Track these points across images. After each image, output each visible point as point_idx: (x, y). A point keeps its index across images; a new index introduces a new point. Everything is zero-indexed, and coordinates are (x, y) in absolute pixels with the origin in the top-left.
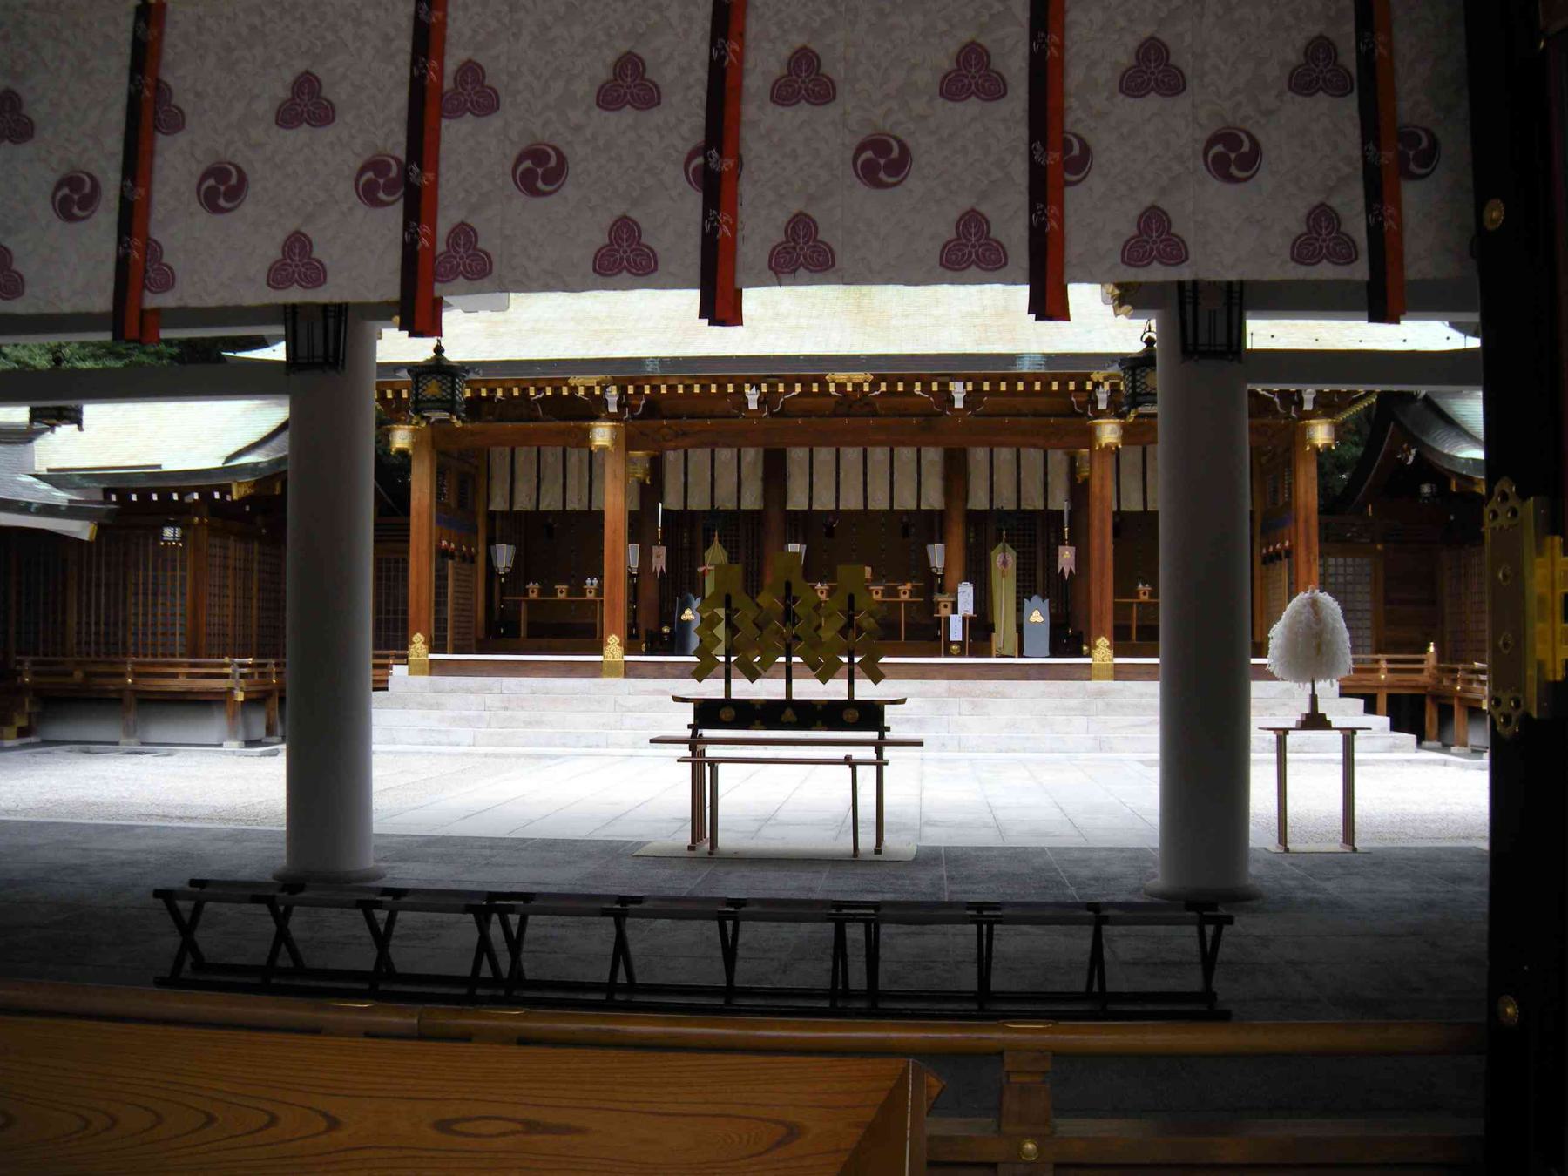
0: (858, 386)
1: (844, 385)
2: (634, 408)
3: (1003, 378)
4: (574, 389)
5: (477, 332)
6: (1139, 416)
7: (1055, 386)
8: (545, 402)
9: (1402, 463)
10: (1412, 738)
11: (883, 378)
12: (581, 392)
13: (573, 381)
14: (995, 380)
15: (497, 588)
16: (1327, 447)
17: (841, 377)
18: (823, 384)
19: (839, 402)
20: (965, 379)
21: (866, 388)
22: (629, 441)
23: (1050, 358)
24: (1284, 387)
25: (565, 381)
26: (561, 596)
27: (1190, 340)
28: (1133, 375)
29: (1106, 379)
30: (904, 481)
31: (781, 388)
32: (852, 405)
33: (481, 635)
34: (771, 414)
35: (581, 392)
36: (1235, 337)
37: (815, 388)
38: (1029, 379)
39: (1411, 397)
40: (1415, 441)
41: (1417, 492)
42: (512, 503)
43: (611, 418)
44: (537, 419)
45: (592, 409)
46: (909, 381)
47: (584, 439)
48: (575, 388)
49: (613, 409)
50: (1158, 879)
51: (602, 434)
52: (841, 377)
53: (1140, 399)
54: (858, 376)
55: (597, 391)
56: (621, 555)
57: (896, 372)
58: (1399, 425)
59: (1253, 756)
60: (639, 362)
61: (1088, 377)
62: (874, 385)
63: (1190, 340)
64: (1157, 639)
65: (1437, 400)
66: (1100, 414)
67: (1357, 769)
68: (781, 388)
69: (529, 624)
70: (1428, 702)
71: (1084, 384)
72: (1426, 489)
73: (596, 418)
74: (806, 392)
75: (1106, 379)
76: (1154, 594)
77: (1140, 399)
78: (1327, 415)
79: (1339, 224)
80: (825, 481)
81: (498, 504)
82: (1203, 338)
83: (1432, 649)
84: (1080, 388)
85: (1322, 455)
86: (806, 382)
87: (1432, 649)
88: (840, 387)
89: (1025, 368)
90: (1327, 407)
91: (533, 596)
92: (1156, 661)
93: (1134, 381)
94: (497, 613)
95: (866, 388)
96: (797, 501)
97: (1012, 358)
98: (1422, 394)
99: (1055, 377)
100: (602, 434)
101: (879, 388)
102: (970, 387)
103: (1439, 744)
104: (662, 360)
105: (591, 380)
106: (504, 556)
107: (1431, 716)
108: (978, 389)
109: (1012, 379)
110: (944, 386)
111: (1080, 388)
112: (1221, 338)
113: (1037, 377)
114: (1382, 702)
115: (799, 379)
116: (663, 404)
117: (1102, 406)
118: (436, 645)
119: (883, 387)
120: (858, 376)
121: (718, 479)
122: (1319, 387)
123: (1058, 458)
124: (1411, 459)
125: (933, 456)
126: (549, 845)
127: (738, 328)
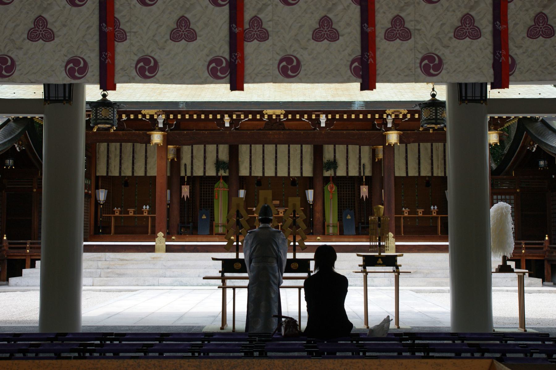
0: (278, 116)
1: (272, 115)
2: (170, 125)
3: (345, 112)
4: (144, 116)
5: (516, 91)
6: (99, 129)
7: (361, 116)
8: (134, 123)
9: (529, 151)
10: (541, 280)
11: (290, 112)
12: (148, 117)
13: (143, 112)
14: (341, 113)
15: (99, 211)
16: (496, 144)
17: (270, 112)
18: (262, 116)
19: (267, 123)
20: (326, 113)
21: (282, 117)
22: (167, 140)
23: (367, 103)
24: (17, 115)
25: (140, 112)
26: (131, 214)
27: (464, 94)
28: (96, 110)
29: (393, 113)
30: (293, 161)
31: (242, 117)
32: (274, 124)
33: (92, 233)
34: (236, 129)
35: (148, 117)
36: (484, 95)
37: (258, 117)
38: (357, 113)
39: (535, 120)
40: (536, 140)
41: (537, 165)
42: (419, 172)
43: (161, 130)
44: (123, 130)
45: (152, 124)
46: (302, 114)
47: (148, 140)
48: (144, 116)
49: (161, 125)
50: (37, 331)
51: (157, 138)
52: (270, 112)
53: (439, 121)
54: (278, 112)
55: (155, 117)
56: (164, 195)
57: (295, 109)
58: (529, 133)
59: (493, 288)
60: (176, 103)
61: (384, 112)
62: (286, 115)
63: (464, 94)
64: (447, 234)
65: (547, 121)
66: (390, 129)
67: (526, 295)
68: (242, 117)
69: (116, 227)
70: (546, 263)
71: (383, 115)
72: (542, 163)
73: (153, 130)
74: (254, 118)
75: (393, 113)
76: (152, 210)
77: (439, 121)
78: (495, 129)
79: (328, 40)
80: (262, 161)
81: (400, 172)
82: (469, 94)
83: (547, 238)
84: (381, 117)
85: (493, 148)
86: (254, 113)
87: (547, 238)
88: (270, 116)
89: (356, 108)
90: (495, 124)
91: (117, 214)
92: (447, 243)
93: (96, 113)
94: (99, 223)
95: (282, 117)
96: (244, 172)
97: (351, 103)
98: (541, 118)
99: (369, 112)
100: (157, 138)
101: (248, 117)
102: (330, 117)
103: (552, 283)
104: (187, 103)
105: (152, 112)
106: (102, 195)
107: (547, 269)
108: (333, 118)
109: (349, 113)
110: (318, 116)
111: (381, 117)
112: (478, 94)
113: (361, 112)
114: (523, 264)
115: (250, 112)
116: (186, 124)
117: (389, 125)
118: (168, 237)
119: (290, 117)
120: (278, 112)
121: (202, 160)
122: (492, 115)
123: (366, 150)
124: (535, 149)
125: (308, 149)
126: (192, 331)
127: (359, 88)
